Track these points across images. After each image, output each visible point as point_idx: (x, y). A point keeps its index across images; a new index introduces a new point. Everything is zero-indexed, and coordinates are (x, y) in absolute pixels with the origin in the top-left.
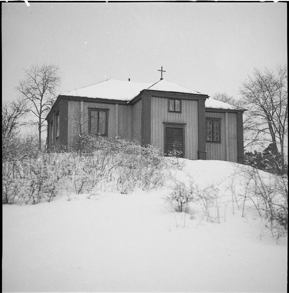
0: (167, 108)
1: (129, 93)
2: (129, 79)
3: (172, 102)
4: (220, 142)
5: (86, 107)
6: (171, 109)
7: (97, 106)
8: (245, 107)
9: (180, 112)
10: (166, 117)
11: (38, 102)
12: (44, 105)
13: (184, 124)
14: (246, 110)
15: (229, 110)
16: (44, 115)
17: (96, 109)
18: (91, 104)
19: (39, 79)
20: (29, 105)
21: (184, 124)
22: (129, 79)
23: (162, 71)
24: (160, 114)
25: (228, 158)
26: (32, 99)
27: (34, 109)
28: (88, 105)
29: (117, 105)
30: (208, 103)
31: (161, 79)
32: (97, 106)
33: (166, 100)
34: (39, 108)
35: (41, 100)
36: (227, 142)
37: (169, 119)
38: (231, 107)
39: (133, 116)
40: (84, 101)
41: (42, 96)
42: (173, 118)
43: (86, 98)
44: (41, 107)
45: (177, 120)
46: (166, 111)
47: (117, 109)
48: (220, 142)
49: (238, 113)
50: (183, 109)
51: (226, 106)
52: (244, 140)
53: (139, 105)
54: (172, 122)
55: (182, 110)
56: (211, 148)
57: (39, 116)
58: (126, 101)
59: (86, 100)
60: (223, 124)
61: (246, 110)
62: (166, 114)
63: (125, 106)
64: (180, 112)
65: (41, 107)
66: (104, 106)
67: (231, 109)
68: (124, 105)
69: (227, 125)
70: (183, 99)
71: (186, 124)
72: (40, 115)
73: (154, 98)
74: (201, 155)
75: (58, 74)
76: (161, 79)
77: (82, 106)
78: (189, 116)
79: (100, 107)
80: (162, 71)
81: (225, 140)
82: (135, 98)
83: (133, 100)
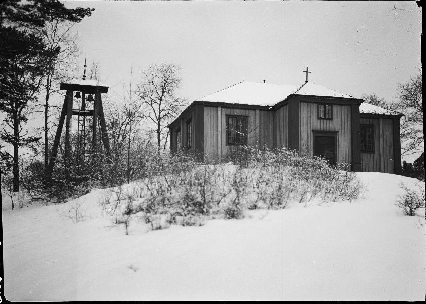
0: (316, 114)
1: (272, 96)
2: (264, 81)
3: (322, 107)
4: (373, 152)
5: (224, 113)
6: (321, 116)
7: (236, 112)
8: (400, 111)
9: (331, 119)
10: (316, 124)
11: (156, 107)
12: (163, 110)
13: (336, 132)
14: (404, 115)
15: (384, 115)
16: (165, 123)
17: (233, 116)
18: (229, 110)
19: (158, 81)
20: (145, 109)
21: (336, 132)
22: (264, 81)
23: (307, 72)
24: (308, 122)
25: (382, 169)
26: (150, 103)
27: (153, 115)
28: (225, 111)
29: (257, 112)
30: (364, 108)
31: (307, 81)
32: (236, 112)
33: (316, 106)
34: (157, 113)
35: (160, 105)
36: (382, 152)
37: (319, 126)
38: (386, 112)
39: (275, 124)
40: (383, 118)
41: (161, 100)
42: (323, 125)
43: (224, 104)
44: (160, 113)
45: (336, 129)
46: (316, 118)
47: (257, 116)
48: (373, 152)
49: (393, 120)
50: (335, 116)
51: (379, 110)
52: (402, 151)
53: (284, 112)
54: (322, 129)
55: (334, 117)
56: (365, 158)
57: (157, 122)
58: (267, 107)
59: (224, 106)
60: (376, 131)
61: (404, 115)
62: (316, 122)
63: (266, 112)
64: (331, 119)
65: (160, 113)
66: (243, 112)
67: (386, 114)
68: (266, 111)
69: (381, 132)
70: (335, 104)
71: (338, 132)
72: (159, 122)
73: (302, 104)
74: (355, 166)
75: (177, 75)
76: (307, 81)
77: (219, 113)
78: (341, 124)
79: (238, 115)
80: (307, 72)
81: (217, 139)
82: (279, 103)
83: (276, 105)
